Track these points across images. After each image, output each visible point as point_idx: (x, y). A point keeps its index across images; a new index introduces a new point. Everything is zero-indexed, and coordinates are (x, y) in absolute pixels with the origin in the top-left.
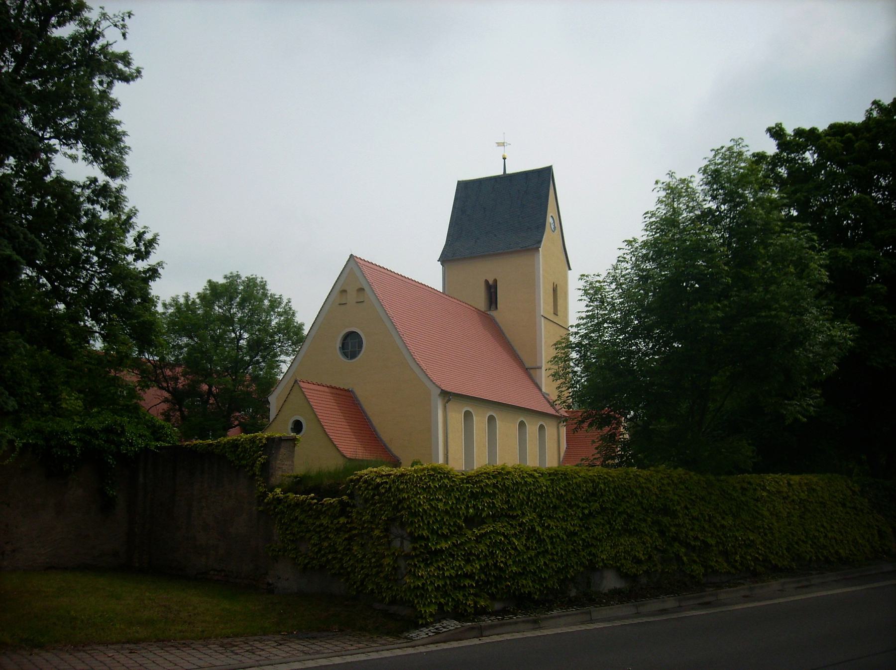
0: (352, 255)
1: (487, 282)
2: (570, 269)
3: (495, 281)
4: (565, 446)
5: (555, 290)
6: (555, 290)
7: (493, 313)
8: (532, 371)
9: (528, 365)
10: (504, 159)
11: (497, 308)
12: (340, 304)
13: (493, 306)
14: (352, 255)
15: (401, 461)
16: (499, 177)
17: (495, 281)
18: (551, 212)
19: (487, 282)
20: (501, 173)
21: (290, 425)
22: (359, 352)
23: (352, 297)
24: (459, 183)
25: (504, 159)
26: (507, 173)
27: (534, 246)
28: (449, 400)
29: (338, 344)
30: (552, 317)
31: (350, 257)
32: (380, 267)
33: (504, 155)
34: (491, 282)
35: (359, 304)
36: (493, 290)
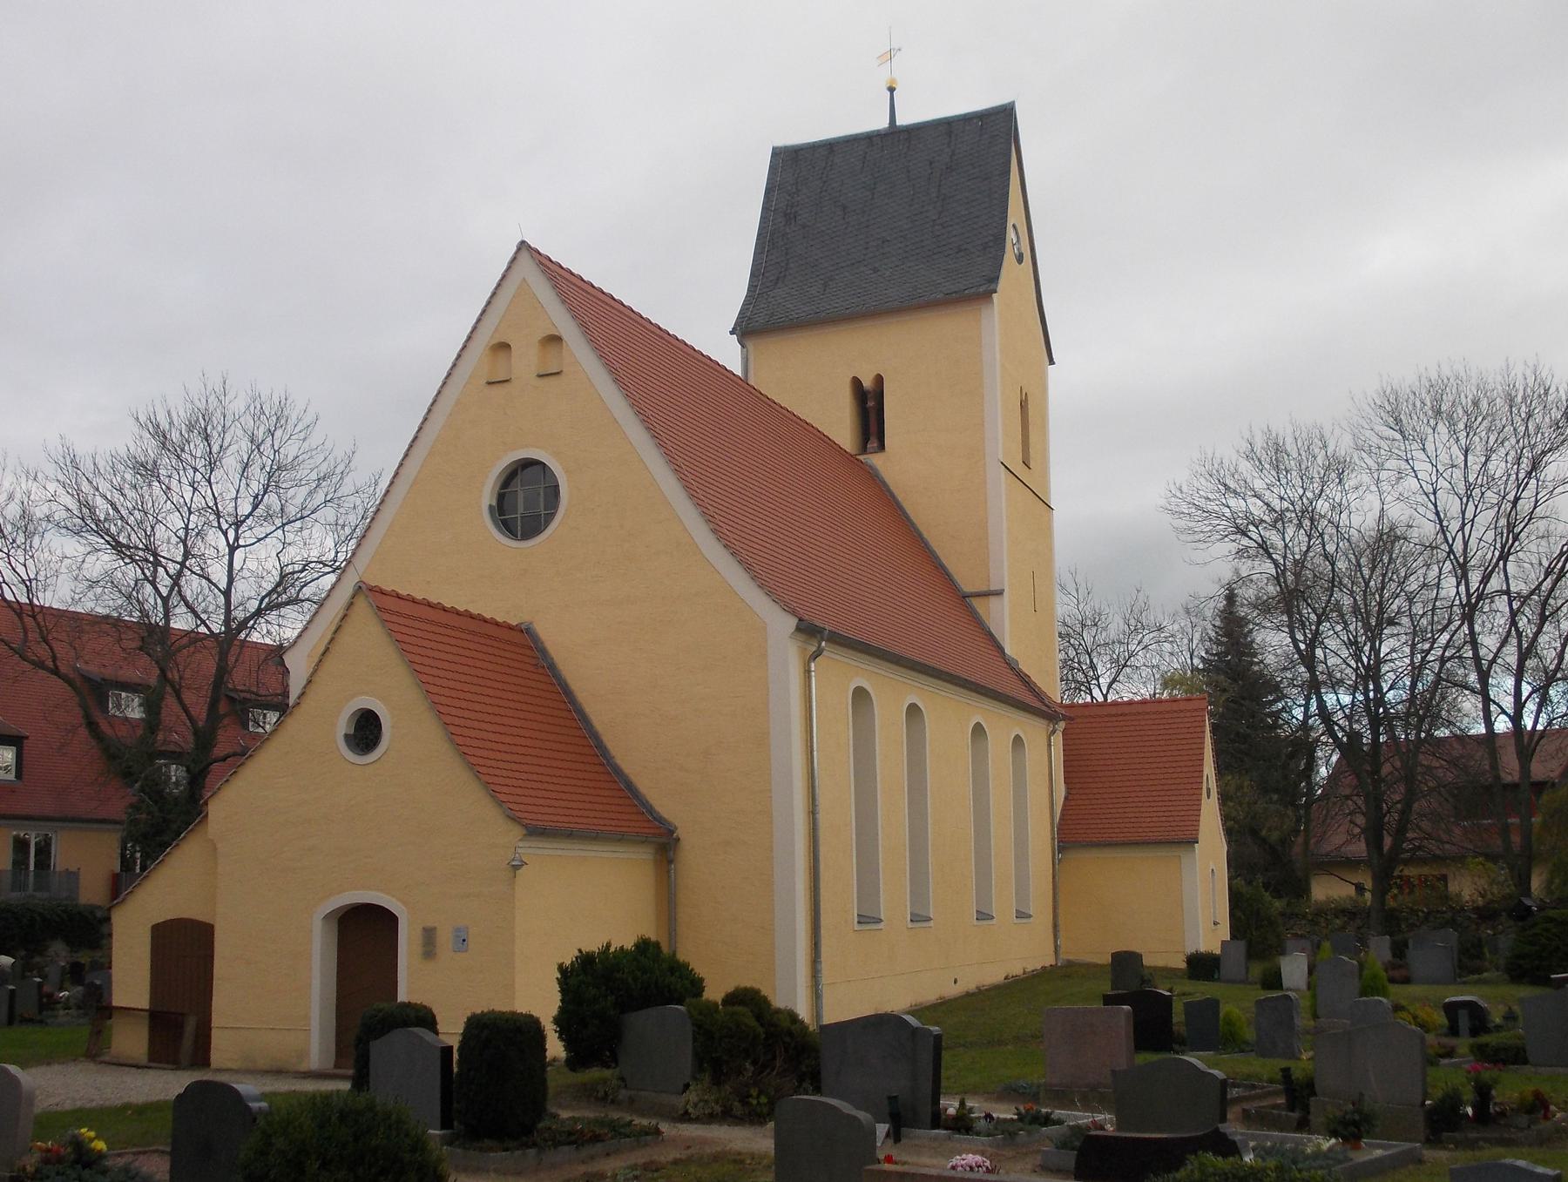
0: (523, 242)
1: (856, 383)
2: (1052, 362)
3: (879, 380)
4: (1063, 794)
5: (1024, 406)
6: (1024, 406)
7: (876, 460)
8: (977, 603)
9: (967, 588)
10: (892, 90)
11: (882, 447)
12: (489, 383)
13: (872, 444)
14: (523, 242)
15: (679, 833)
16: (870, 139)
17: (879, 380)
18: (1014, 216)
19: (856, 383)
20: (882, 123)
21: (343, 725)
22: (550, 517)
23: (525, 360)
24: (776, 153)
25: (892, 90)
26: (898, 124)
27: (979, 288)
28: (816, 655)
29: (487, 497)
30: (1019, 469)
31: (519, 249)
32: (414, 601)
33: (893, 81)
34: (867, 383)
35: (546, 380)
36: (871, 404)
